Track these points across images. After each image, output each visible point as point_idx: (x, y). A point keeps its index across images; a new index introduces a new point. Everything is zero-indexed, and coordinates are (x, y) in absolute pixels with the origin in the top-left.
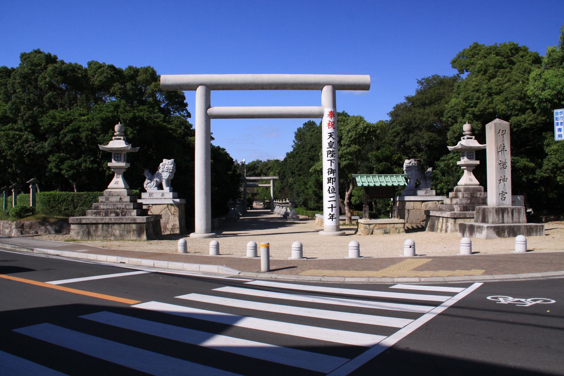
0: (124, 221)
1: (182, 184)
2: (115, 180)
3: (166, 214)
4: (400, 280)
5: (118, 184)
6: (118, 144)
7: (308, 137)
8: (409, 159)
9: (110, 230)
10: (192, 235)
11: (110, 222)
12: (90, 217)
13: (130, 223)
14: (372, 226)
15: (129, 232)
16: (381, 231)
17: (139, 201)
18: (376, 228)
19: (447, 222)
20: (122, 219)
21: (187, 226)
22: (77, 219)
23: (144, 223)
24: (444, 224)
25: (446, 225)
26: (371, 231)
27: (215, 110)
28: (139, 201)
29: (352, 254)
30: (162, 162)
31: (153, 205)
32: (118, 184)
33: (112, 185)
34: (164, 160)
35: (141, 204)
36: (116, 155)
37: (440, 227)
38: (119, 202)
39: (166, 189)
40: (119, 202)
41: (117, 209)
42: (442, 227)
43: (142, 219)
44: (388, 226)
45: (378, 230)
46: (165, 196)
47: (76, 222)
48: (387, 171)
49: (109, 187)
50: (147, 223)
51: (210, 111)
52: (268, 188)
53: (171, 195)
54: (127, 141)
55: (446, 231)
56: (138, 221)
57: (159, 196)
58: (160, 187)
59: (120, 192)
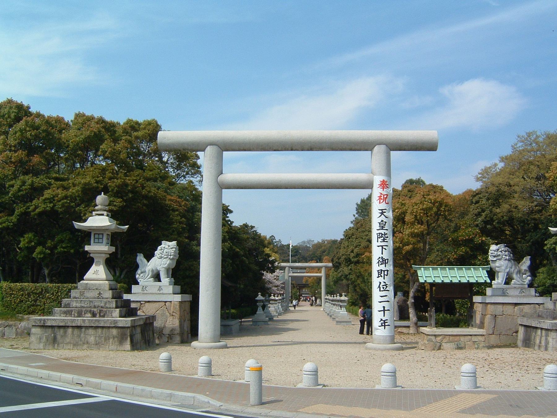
1: (185, 274)
2: (94, 268)
3: (163, 315)
5: (97, 274)
6: (99, 221)
8: (497, 244)
9: (82, 335)
10: (194, 344)
12: (57, 317)
13: (109, 327)
14: (439, 338)
15: (107, 339)
16: (452, 345)
17: (126, 297)
18: (445, 341)
19: (547, 336)
20: (98, 321)
21: (190, 332)
22: (40, 320)
23: (128, 327)
24: (543, 338)
25: (546, 339)
26: (438, 344)
27: (229, 176)
28: (126, 297)
29: (384, 384)
30: (161, 244)
31: (146, 302)
32: (97, 274)
34: (163, 242)
35: (128, 302)
36: (97, 236)
37: (538, 341)
38: (98, 298)
39: (165, 280)
40: (98, 298)
41: (95, 307)
42: (540, 342)
43: (127, 321)
44: (462, 338)
45: (449, 344)
46: (165, 291)
47: (38, 324)
48: (464, 261)
49: (85, 277)
50: (133, 327)
51: (221, 178)
53: (170, 289)
54: (114, 215)
55: (546, 349)
57: (155, 290)
58: (157, 277)
59: (100, 284)
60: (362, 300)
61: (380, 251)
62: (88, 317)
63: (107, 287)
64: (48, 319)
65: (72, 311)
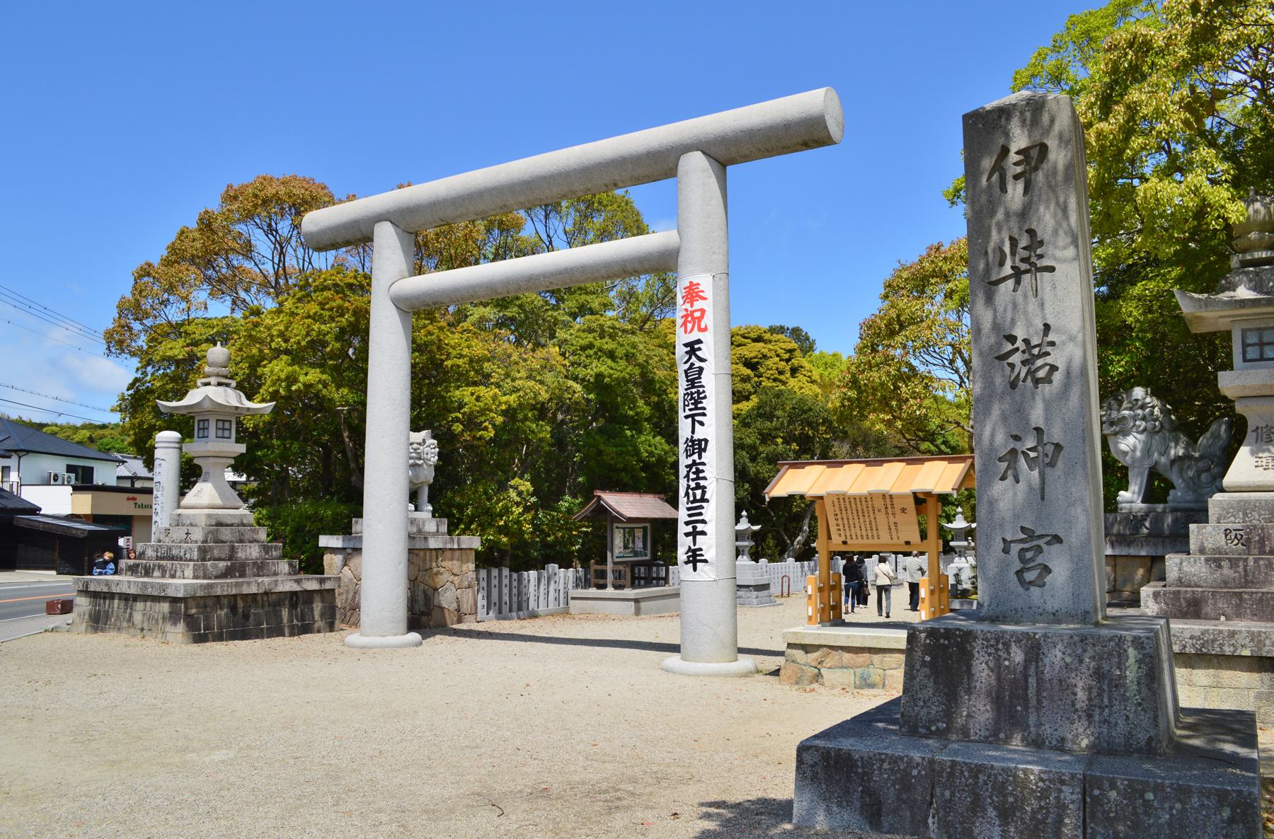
0: (149, 591)
18: (829, 662)
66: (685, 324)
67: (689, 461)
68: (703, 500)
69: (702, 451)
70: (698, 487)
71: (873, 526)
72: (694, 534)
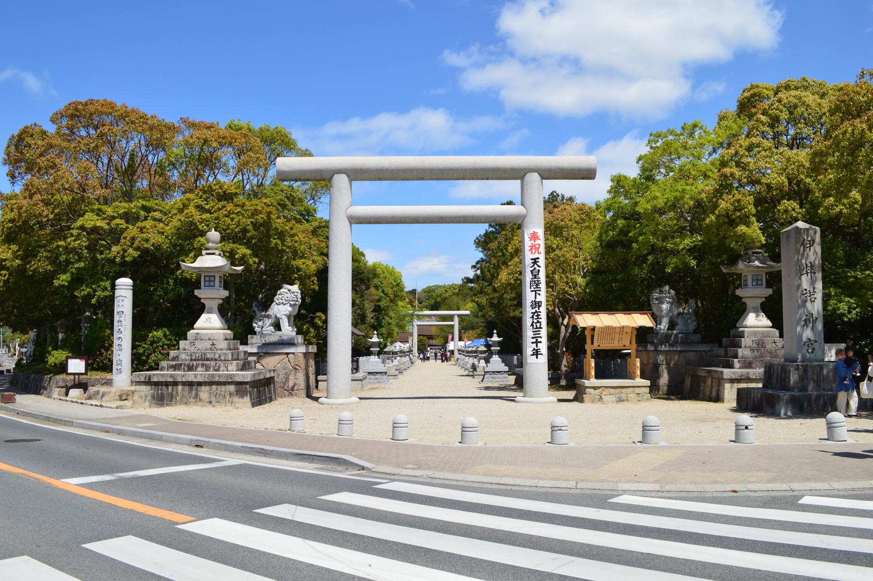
0: (217, 379)
2: (204, 316)
4: (627, 486)
5: (210, 323)
7: (499, 240)
11: (195, 380)
18: (604, 393)
20: (213, 376)
32: (210, 323)
33: (200, 323)
49: (195, 326)
52: (452, 326)
56: (238, 379)
60: (511, 347)
61: (536, 300)
62: (200, 371)
63: (222, 337)
64: (154, 375)
65: (181, 365)
66: (531, 250)
67: (534, 311)
68: (540, 328)
69: (539, 306)
70: (538, 322)
71: (613, 339)
72: (537, 342)
